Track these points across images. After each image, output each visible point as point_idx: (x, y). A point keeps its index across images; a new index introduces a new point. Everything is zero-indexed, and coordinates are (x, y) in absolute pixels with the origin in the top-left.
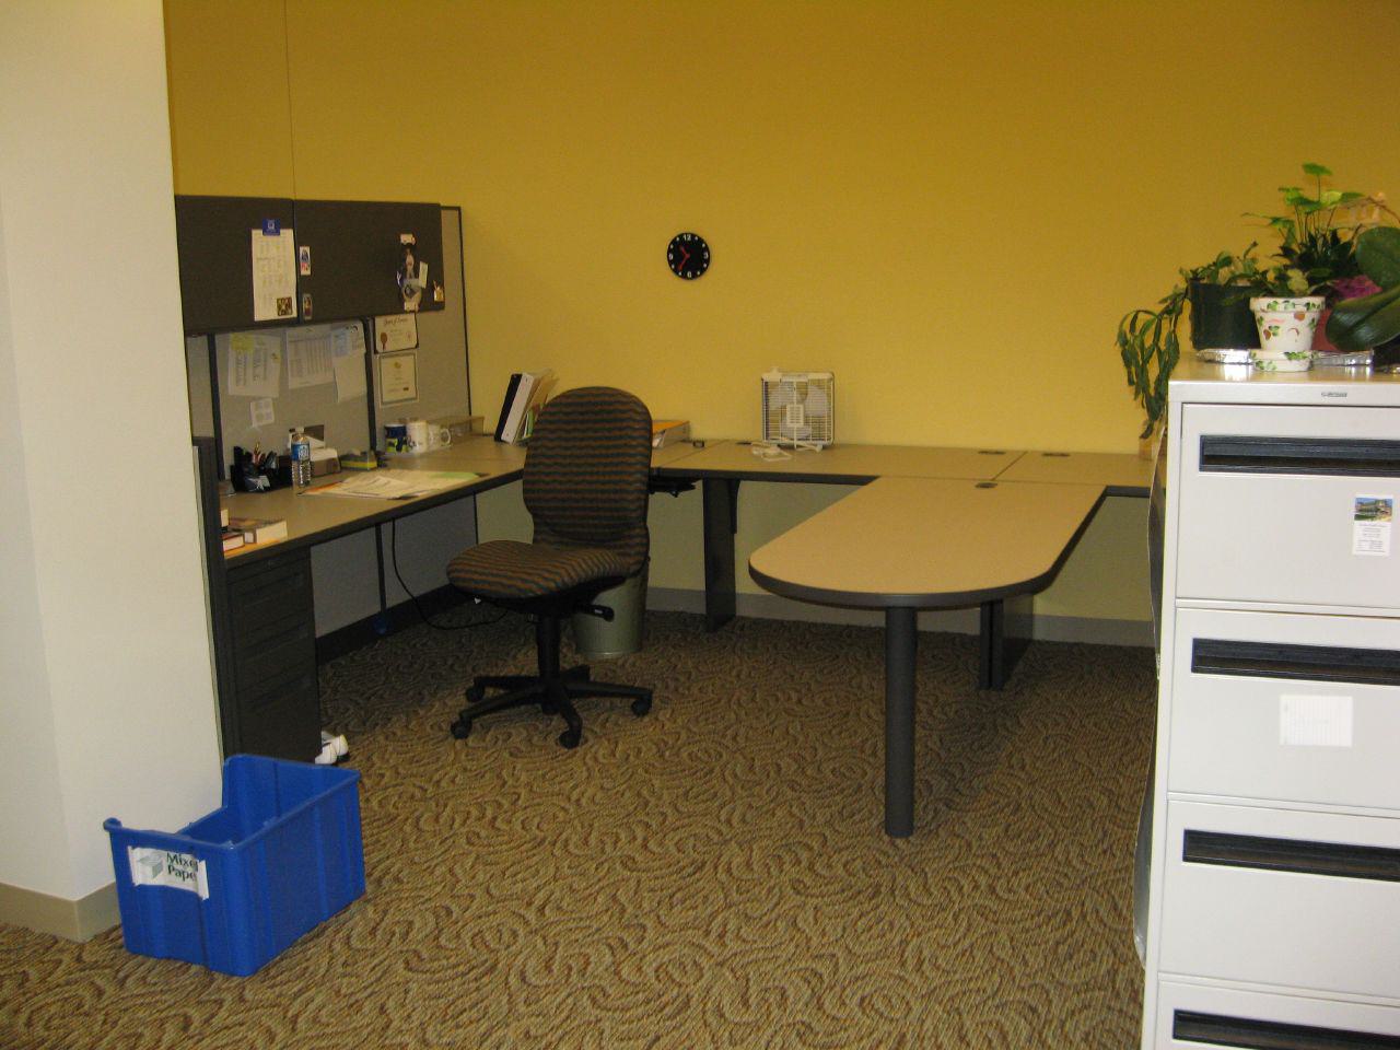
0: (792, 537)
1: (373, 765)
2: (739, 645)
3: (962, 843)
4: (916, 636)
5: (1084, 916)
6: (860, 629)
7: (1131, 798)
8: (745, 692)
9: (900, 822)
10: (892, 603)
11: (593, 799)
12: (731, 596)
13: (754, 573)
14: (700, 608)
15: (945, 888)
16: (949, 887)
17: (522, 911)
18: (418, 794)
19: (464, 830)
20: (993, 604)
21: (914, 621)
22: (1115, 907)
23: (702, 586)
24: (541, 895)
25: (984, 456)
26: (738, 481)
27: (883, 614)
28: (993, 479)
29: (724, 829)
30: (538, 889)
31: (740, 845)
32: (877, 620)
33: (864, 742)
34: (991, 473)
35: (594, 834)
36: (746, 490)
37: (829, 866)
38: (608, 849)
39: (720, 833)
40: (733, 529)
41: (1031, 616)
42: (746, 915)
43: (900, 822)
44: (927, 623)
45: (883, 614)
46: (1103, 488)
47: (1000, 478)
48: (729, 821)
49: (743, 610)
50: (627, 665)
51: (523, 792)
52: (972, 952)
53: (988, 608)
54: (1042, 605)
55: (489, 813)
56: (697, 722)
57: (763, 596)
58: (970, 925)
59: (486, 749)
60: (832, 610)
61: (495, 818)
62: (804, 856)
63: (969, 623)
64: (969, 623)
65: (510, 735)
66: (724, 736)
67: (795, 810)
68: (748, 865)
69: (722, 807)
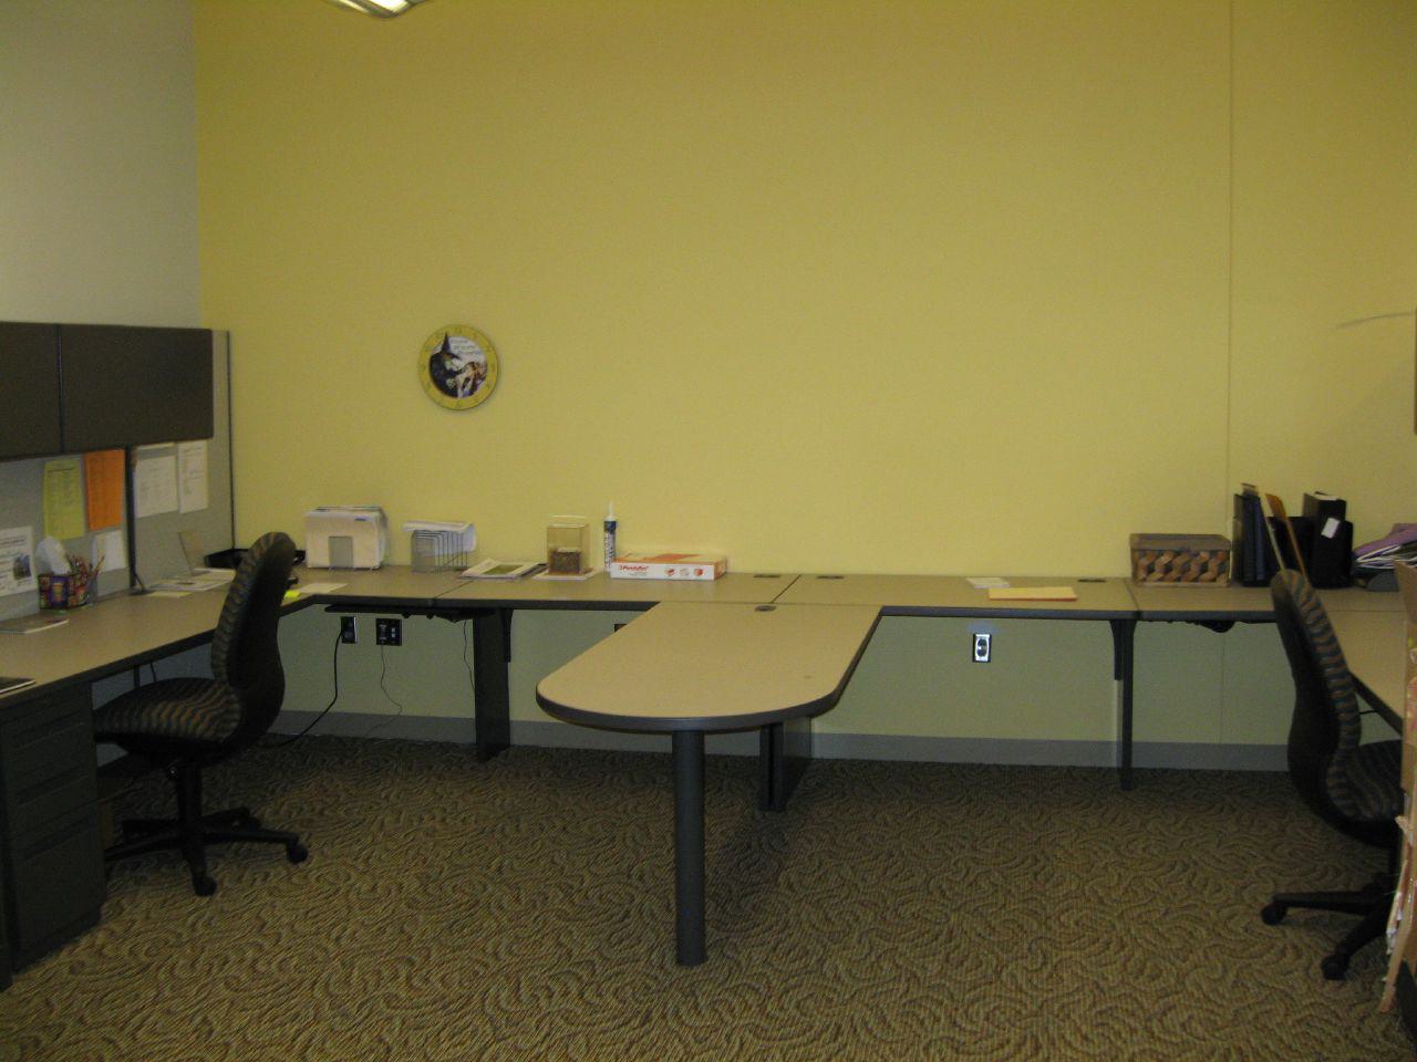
0: (568, 669)
1: (123, 910)
2: (615, 780)
3: (732, 963)
4: (703, 760)
5: (664, 1016)
6: (625, 754)
7: (896, 910)
8: (509, 822)
9: (690, 949)
10: (680, 727)
11: (353, 937)
12: (505, 722)
13: (544, 704)
14: (469, 737)
15: (716, 1011)
16: (720, 1009)
17: (113, 1037)
18: (173, 940)
19: (221, 975)
20: (772, 727)
21: (702, 743)
22: (884, 1019)
23: (474, 717)
24: (137, 1019)
25: (825, 581)
26: (511, 610)
27: (670, 737)
28: (772, 602)
29: (491, 961)
30: (299, 1033)
31: (508, 978)
32: (663, 745)
33: (631, 868)
34: (770, 596)
35: (356, 973)
36: (521, 622)
37: (600, 995)
38: (543, 1002)
39: (486, 966)
40: (507, 658)
41: (810, 734)
42: (516, 1047)
43: (690, 949)
44: (714, 745)
45: (670, 737)
46: (878, 610)
47: (778, 600)
48: (496, 954)
49: (517, 739)
50: (392, 797)
51: (284, 932)
52: (546, 1055)
53: (767, 731)
54: (819, 726)
55: (250, 954)
56: (461, 855)
57: (542, 724)
58: (742, 1045)
59: (243, 890)
60: (605, 734)
61: (255, 961)
62: (751, 998)
63: (750, 745)
64: (750, 745)
65: (267, 875)
66: (629, 877)
67: (563, 939)
68: (347, 982)
69: (487, 939)
